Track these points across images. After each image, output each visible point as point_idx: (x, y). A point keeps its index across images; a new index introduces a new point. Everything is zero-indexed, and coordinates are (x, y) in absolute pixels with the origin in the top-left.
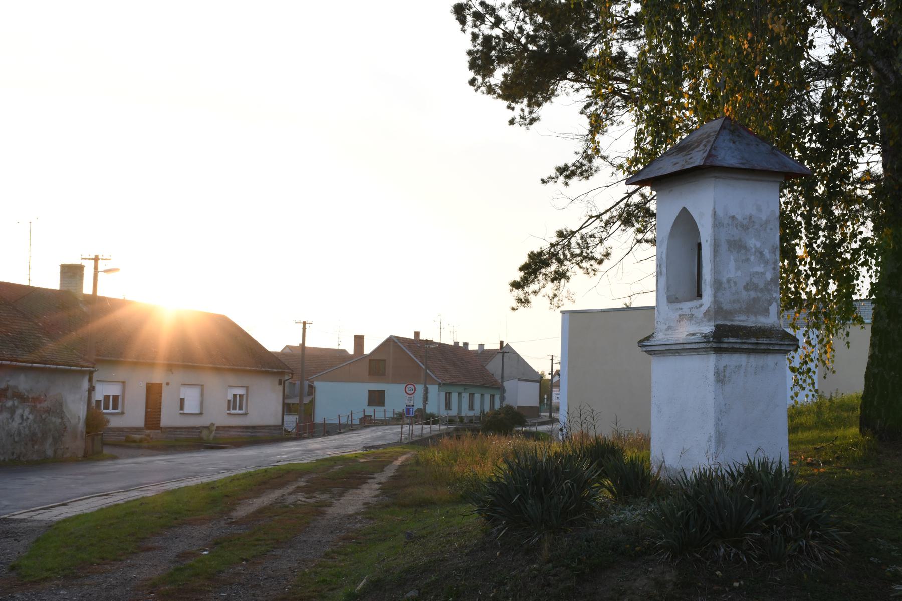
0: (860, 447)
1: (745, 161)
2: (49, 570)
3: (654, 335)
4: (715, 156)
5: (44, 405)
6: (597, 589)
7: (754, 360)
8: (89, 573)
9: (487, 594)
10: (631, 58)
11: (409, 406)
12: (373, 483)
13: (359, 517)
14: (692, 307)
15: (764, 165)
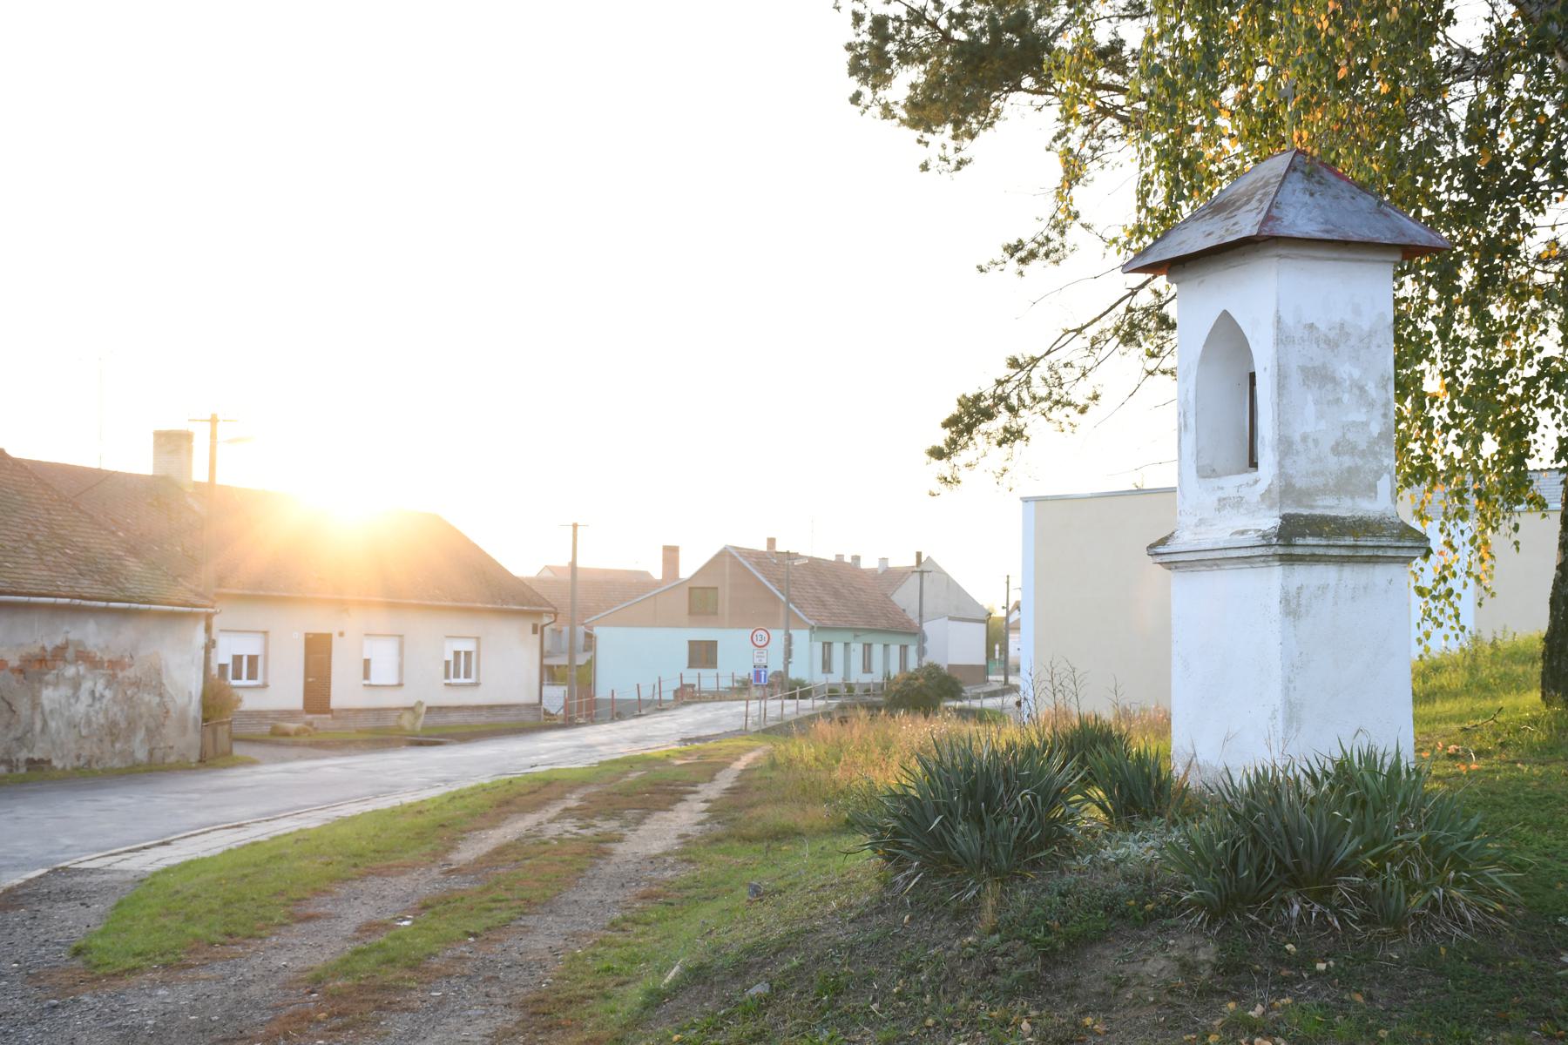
0: (1542, 724)
1: (1331, 227)
2: (140, 954)
3: (1175, 535)
4: (1278, 219)
5: (130, 673)
6: (1078, 977)
7: (1352, 576)
8: (206, 958)
9: (887, 988)
10: (1133, 51)
11: (759, 667)
12: (694, 800)
13: (671, 860)
15: (1366, 234)
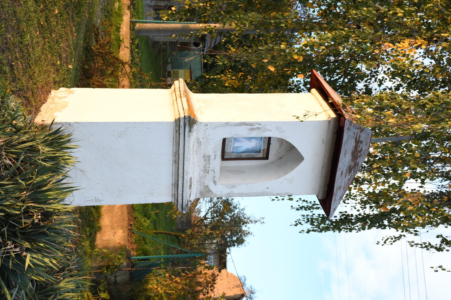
14: (214, 172)
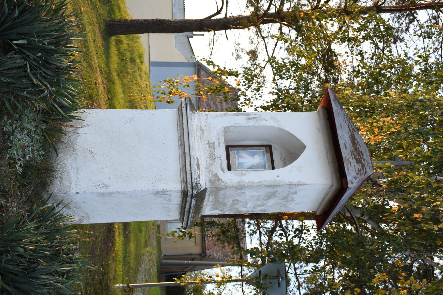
14: (221, 159)
